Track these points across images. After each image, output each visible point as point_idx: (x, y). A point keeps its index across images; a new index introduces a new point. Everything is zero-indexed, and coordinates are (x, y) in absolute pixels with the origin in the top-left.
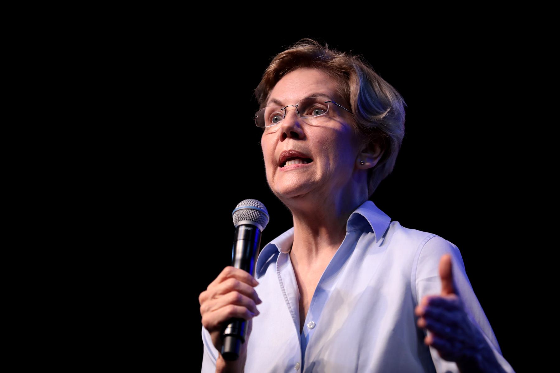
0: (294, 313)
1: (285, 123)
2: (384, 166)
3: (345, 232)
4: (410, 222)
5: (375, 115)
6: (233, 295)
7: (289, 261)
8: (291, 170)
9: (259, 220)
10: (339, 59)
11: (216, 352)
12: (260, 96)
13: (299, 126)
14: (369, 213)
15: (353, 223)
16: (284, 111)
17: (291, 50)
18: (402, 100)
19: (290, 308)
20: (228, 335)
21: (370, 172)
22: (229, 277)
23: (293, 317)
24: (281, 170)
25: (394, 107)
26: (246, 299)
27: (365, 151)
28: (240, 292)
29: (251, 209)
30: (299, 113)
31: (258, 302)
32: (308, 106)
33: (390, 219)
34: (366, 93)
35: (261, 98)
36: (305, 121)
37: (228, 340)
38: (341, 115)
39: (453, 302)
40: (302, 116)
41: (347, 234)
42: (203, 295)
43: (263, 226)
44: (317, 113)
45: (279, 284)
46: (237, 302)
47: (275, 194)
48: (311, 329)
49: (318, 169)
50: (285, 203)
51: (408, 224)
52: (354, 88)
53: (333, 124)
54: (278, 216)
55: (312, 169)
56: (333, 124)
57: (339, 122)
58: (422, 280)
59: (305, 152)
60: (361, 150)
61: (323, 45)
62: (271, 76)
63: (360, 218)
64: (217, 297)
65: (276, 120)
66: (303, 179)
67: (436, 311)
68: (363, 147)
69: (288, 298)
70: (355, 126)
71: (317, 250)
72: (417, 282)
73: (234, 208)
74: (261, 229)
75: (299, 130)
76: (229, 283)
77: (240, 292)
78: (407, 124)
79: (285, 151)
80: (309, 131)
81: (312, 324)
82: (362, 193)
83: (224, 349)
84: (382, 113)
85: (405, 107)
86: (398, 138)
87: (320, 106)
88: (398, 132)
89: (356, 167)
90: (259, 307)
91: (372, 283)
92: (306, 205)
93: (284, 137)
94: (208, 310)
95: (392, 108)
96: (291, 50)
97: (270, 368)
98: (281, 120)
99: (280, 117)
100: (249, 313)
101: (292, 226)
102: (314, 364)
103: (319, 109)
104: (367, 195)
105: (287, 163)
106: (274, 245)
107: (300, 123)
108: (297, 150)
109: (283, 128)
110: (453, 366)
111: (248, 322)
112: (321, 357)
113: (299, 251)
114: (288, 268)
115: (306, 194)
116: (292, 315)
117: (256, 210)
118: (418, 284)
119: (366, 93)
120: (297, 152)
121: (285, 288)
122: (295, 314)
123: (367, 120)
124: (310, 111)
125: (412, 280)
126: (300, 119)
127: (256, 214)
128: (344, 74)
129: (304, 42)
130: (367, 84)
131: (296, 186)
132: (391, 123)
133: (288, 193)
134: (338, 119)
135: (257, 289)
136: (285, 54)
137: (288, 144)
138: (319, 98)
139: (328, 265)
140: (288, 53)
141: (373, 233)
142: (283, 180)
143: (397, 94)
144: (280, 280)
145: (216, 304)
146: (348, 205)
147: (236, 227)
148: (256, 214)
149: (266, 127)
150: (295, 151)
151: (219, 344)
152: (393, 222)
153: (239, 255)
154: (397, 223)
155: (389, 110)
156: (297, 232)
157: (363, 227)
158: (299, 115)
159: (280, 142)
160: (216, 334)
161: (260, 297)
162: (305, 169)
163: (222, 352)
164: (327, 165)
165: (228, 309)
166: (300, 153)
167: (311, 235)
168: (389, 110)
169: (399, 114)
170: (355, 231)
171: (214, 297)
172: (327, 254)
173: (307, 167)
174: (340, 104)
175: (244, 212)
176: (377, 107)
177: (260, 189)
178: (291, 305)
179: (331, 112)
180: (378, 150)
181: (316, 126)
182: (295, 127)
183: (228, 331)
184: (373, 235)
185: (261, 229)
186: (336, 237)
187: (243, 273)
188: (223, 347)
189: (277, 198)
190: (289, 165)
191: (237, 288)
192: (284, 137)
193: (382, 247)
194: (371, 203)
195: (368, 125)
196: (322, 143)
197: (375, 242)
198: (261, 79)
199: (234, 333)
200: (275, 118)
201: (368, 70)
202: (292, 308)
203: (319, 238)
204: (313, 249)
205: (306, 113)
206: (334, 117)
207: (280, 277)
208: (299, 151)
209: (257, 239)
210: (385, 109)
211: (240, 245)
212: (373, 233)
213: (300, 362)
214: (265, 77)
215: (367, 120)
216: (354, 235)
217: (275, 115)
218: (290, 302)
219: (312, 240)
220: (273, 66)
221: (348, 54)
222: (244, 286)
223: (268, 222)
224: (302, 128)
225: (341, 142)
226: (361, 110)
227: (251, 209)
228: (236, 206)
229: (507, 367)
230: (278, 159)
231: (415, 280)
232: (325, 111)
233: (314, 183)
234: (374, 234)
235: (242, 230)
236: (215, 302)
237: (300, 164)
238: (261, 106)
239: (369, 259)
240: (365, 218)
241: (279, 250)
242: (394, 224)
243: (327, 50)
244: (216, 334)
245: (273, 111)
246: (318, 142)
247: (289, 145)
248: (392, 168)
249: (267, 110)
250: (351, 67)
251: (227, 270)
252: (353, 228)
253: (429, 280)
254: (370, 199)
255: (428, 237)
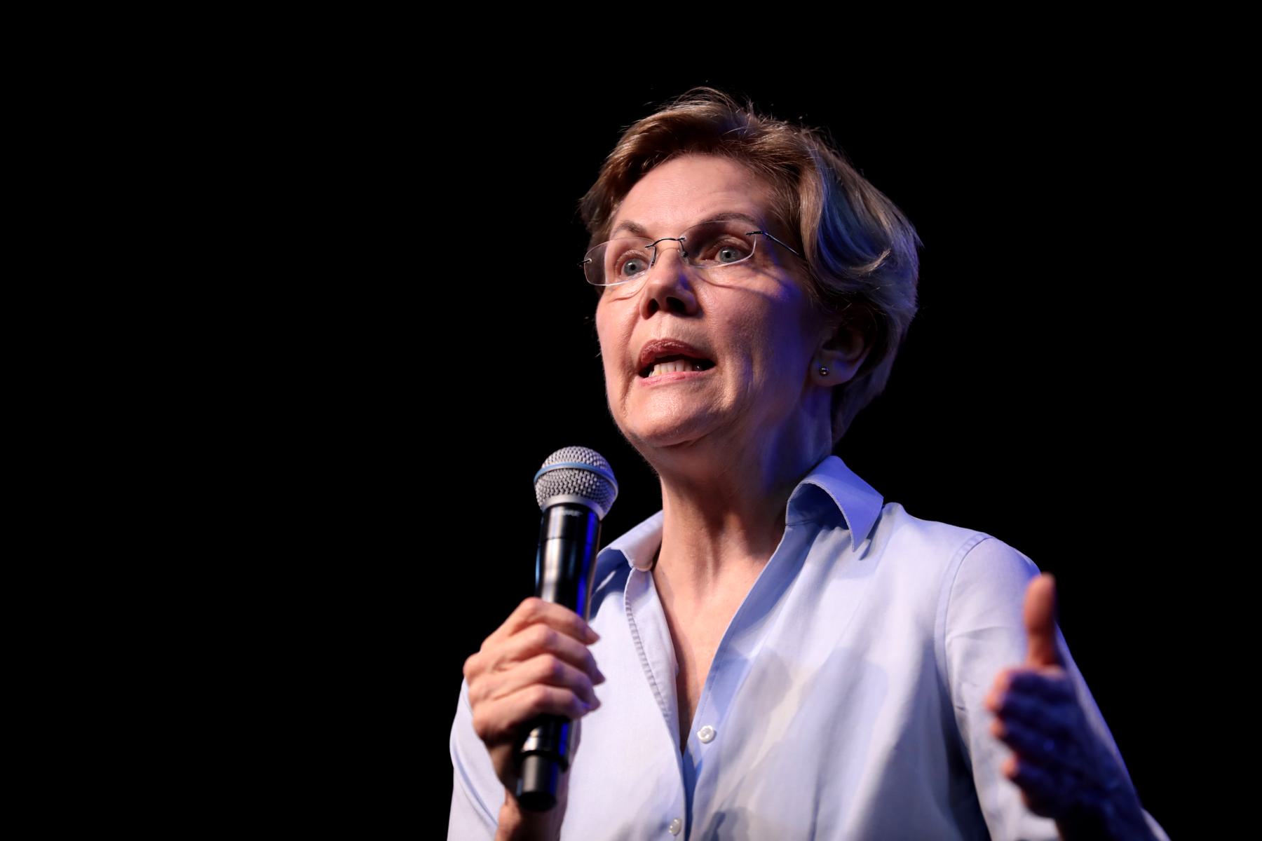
0: (666, 706)
1: (655, 277)
2: (868, 378)
3: (783, 525)
4: (928, 506)
5: (856, 265)
6: (543, 663)
7: (652, 590)
8: (667, 385)
9: (595, 495)
10: (775, 135)
11: (499, 790)
12: (591, 216)
13: (687, 285)
14: (836, 483)
15: (800, 506)
16: (652, 252)
17: (668, 113)
18: (912, 231)
19: (657, 694)
20: (530, 753)
21: (839, 393)
22: (534, 623)
23: (665, 716)
24: (644, 384)
25: (897, 248)
26: (571, 672)
27: (829, 345)
28: (559, 655)
29: (579, 470)
30: (686, 255)
31: (598, 678)
32: (706, 240)
33: (879, 499)
34: (836, 212)
35: (594, 219)
36: (701, 273)
37: (532, 765)
38: (780, 264)
39: (1060, 683)
40: (692, 263)
41: (787, 529)
42: (472, 663)
43: (604, 507)
44: (728, 255)
45: (632, 642)
46: (552, 679)
47: (627, 436)
48: (706, 743)
49: (727, 385)
50: (647, 458)
51: (923, 509)
52: (810, 202)
53: (762, 283)
54: (632, 484)
55: (714, 383)
56: (762, 283)
57: (774, 278)
58: (961, 636)
59: (698, 345)
60: (823, 343)
61: (743, 104)
62: (621, 170)
63: (817, 495)
64: (504, 666)
65: (633, 270)
66: (694, 406)
67: (1027, 703)
68: (827, 336)
69: (654, 672)
70: (811, 290)
71: (717, 564)
72: (948, 639)
73: (539, 467)
74: (601, 513)
75: (687, 294)
76: (534, 634)
77: (559, 655)
78: (922, 287)
79: (654, 342)
80: (709, 298)
81: (708, 731)
82: (820, 439)
83: (523, 785)
84: (871, 262)
85: (919, 249)
86: (902, 316)
87: (733, 240)
88: (904, 302)
89: (809, 381)
90: (598, 690)
91: (846, 642)
92: (695, 465)
93: (651, 308)
94: (486, 696)
95: (892, 251)
96: (668, 113)
97: (614, 829)
98: (644, 269)
99: (643, 264)
100: (580, 703)
101: (657, 506)
102: (720, 818)
103: (732, 247)
104: (829, 443)
105: (657, 368)
106: (619, 553)
107: (690, 278)
108: (680, 339)
109: (650, 290)
110: (1046, 827)
111: (575, 723)
112: (737, 805)
113: (675, 564)
114: (650, 603)
115: (699, 440)
116: (663, 710)
117: (591, 472)
118: (950, 644)
119: (836, 212)
120: (681, 343)
121: (646, 649)
122: (670, 709)
123: (839, 277)
124: (710, 252)
125: (937, 634)
126: (689, 269)
127: (589, 479)
128: (788, 171)
129: (694, 96)
130: (838, 190)
131: (679, 422)
132: (890, 284)
133: (658, 436)
134: (773, 271)
135: (594, 649)
136: (654, 120)
137: (660, 325)
138: (733, 224)
139: (741, 603)
140: (663, 120)
141: (846, 527)
142: (647, 407)
143: (901, 216)
144: (633, 632)
145: (504, 682)
146: (789, 465)
147: (543, 509)
148: (589, 479)
149: (607, 285)
150: (677, 342)
151: (510, 773)
152: (887, 506)
153: (552, 573)
154: (898, 509)
155: (885, 254)
156: (670, 522)
157: (824, 514)
158: (687, 259)
159: (641, 320)
160: (502, 750)
161: (602, 667)
162: (698, 384)
163: (519, 792)
164: (746, 374)
165: (532, 695)
166: (687, 346)
167: (704, 531)
168: (885, 254)
169: (907, 263)
170: (805, 523)
171: (498, 667)
172: (739, 574)
173: (701, 379)
174: (778, 237)
175: (561, 475)
176: (860, 248)
177: (598, 429)
178: (660, 688)
179: (759, 256)
180: (860, 341)
181: (725, 287)
182: (679, 287)
183: (531, 744)
184: (845, 533)
185: (601, 513)
186: (761, 538)
187: (562, 614)
188: (519, 783)
189: (629, 446)
190: (662, 372)
191: (552, 648)
192: (651, 308)
193: (867, 561)
194: (836, 462)
195: (840, 286)
196: (738, 326)
197: (851, 548)
198: (597, 177)
199: (547, 749)
200: (631, 265)
201: (839, 162)
202: (663, 694)
203: (723, 538)
204: (707, 563)
205: (701, 255)
206: (765, 266)
207: (633, 624)
208: (686, 341)
209: (585, 535)
210: (878, 252)
211: (553, 549)
212: (846, 527)
213: (682, 816)
214: (607, 171)
215: (839, 277)
216: (804, 532)
217: (629, 259)
218: (657, 681)
219: (706, 542)
220: (626, 147)
221: (794, 124)
222: (567, 642)
223: (614, 499)
224: (693, 291)
225: (767, 328)
226: (825, 252)
227: (579, 470)
228: (543, 461)
229: (1159, 832)
230: (636, 358)
231: (944, 637)
232: (745, 253)
233: (717, 415)
234: (850, 531)
235: (557, 517)
236: (499, 677)
237: (688, 373)
238: (595, 235)
239: (836, 588)
240: (828, 495)
241: (631, 564)
242: (890, 512)
243: (750, 117)
244: (502, 750)
245: (625, 248)
246: (729, 322)
247: (663, 327)
248: (884, 383)
249: (611, 247)
250: (802, 155)
251: (527, 605)
252: (801, 518)
253: (976, 635)
254: (837, 451)
255: (972, 539)
